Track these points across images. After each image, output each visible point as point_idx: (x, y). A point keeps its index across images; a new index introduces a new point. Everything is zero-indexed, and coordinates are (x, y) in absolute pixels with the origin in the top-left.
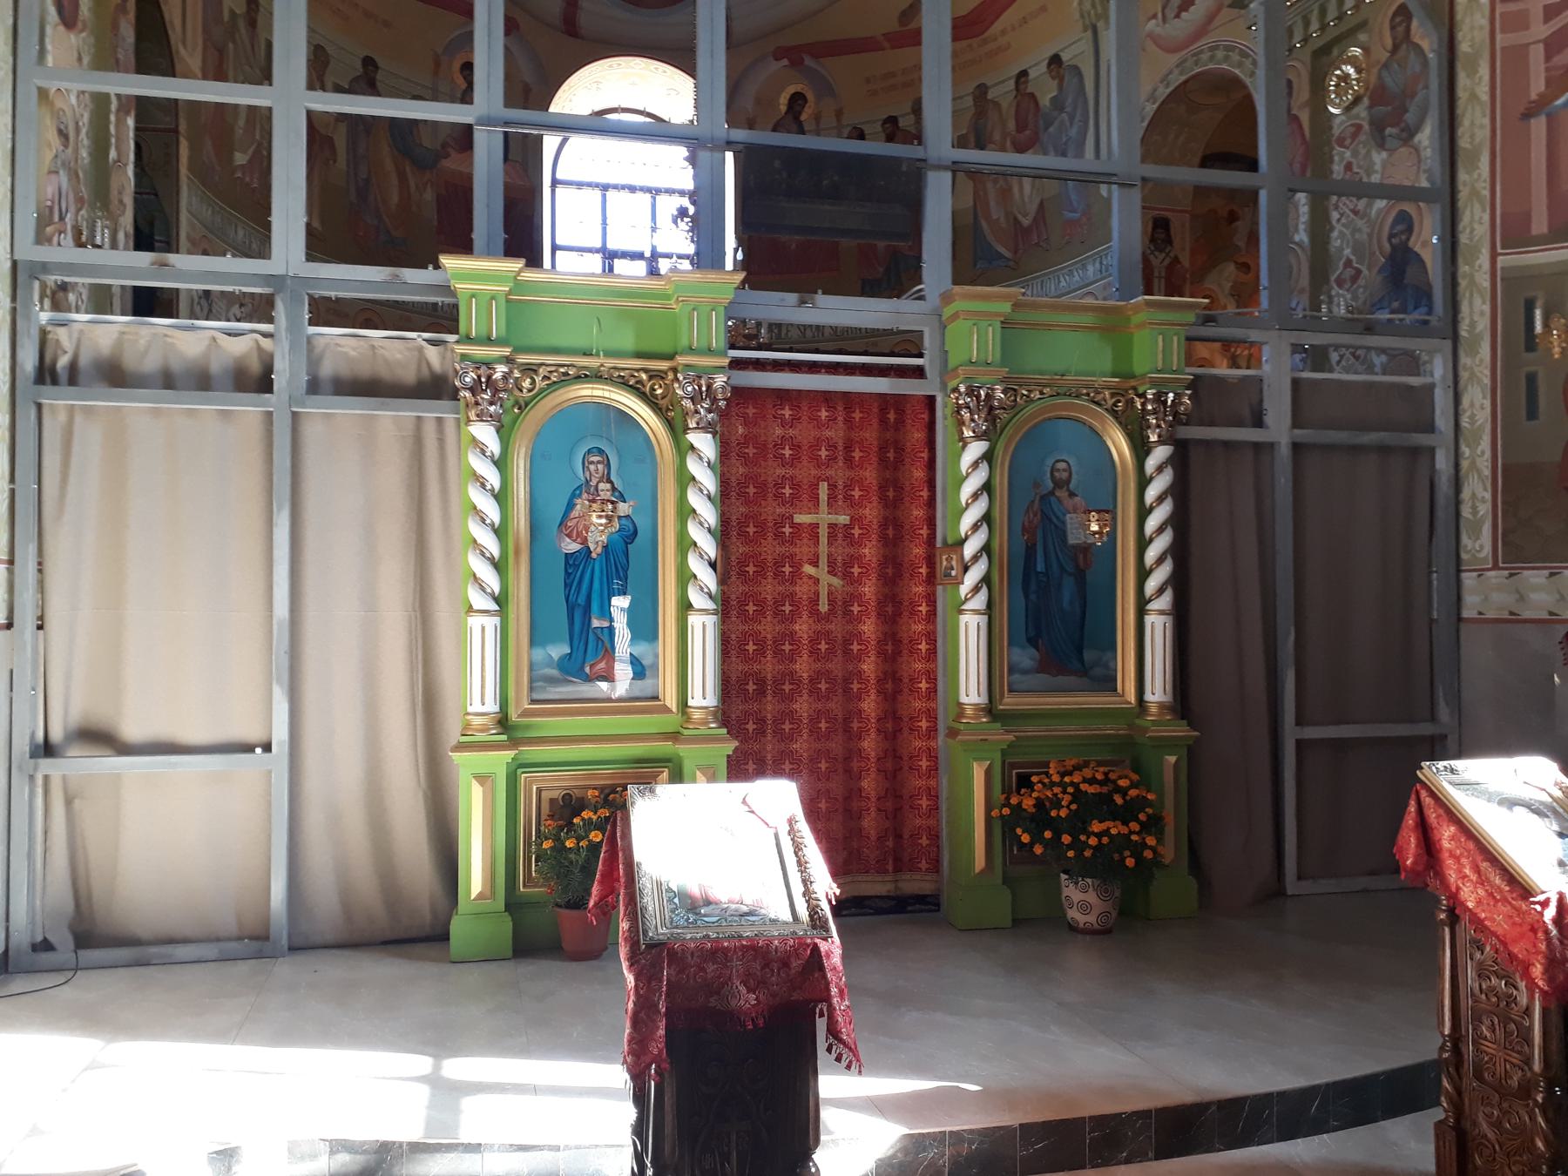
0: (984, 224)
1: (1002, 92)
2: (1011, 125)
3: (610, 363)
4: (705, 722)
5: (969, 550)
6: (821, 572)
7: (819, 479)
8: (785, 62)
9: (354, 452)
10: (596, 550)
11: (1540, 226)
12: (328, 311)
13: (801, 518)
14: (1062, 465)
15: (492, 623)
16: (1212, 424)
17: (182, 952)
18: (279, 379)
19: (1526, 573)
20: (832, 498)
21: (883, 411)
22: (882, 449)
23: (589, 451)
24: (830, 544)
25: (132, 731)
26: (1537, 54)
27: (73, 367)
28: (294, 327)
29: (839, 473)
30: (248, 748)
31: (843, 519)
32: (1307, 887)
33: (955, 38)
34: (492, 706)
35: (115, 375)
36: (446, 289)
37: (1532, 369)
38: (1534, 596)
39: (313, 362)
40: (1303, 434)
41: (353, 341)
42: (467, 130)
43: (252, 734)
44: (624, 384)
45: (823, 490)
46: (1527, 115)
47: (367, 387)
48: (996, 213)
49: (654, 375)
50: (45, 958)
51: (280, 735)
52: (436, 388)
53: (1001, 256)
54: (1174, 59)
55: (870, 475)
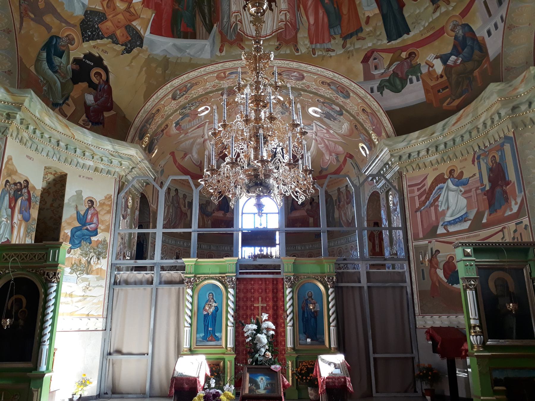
1: (343, 189)
2: (345, 197)
3: (214, 275)
4: (230, 351)
5: (288, 312)
9: (168, 294)
10: (210, 314)
11: (421, 236)
12: (163, 269)
13: (255, 305)
15: (188, 329)
16: (348, 282)
17: (130, 396)
18: (154, 282)
19: (443, 316)
20: (262, 301)
21: (273, 281)
22: (273, 290)
25: (125, 351)
26: (417, 198)
27: (120, 281)
28: (157, 272)
29: (264, 295)
30: (144, 354)
31: (265, 305)
32: (378, 395)
34: (188, 346)
35: (127, 283)
38: (428, 322)
39: (161, 278)
40: (369, 284)
42: (191, 233)
43: (145, 352)
44: (216, 279)
45: (260, 299)
46: (416, 212)
47: (170, 283)
48: (344, 219)
49: (223, 277)
50: (106, 396)
51: (150, 352)
52: (181, 282)
55: (270, 295)
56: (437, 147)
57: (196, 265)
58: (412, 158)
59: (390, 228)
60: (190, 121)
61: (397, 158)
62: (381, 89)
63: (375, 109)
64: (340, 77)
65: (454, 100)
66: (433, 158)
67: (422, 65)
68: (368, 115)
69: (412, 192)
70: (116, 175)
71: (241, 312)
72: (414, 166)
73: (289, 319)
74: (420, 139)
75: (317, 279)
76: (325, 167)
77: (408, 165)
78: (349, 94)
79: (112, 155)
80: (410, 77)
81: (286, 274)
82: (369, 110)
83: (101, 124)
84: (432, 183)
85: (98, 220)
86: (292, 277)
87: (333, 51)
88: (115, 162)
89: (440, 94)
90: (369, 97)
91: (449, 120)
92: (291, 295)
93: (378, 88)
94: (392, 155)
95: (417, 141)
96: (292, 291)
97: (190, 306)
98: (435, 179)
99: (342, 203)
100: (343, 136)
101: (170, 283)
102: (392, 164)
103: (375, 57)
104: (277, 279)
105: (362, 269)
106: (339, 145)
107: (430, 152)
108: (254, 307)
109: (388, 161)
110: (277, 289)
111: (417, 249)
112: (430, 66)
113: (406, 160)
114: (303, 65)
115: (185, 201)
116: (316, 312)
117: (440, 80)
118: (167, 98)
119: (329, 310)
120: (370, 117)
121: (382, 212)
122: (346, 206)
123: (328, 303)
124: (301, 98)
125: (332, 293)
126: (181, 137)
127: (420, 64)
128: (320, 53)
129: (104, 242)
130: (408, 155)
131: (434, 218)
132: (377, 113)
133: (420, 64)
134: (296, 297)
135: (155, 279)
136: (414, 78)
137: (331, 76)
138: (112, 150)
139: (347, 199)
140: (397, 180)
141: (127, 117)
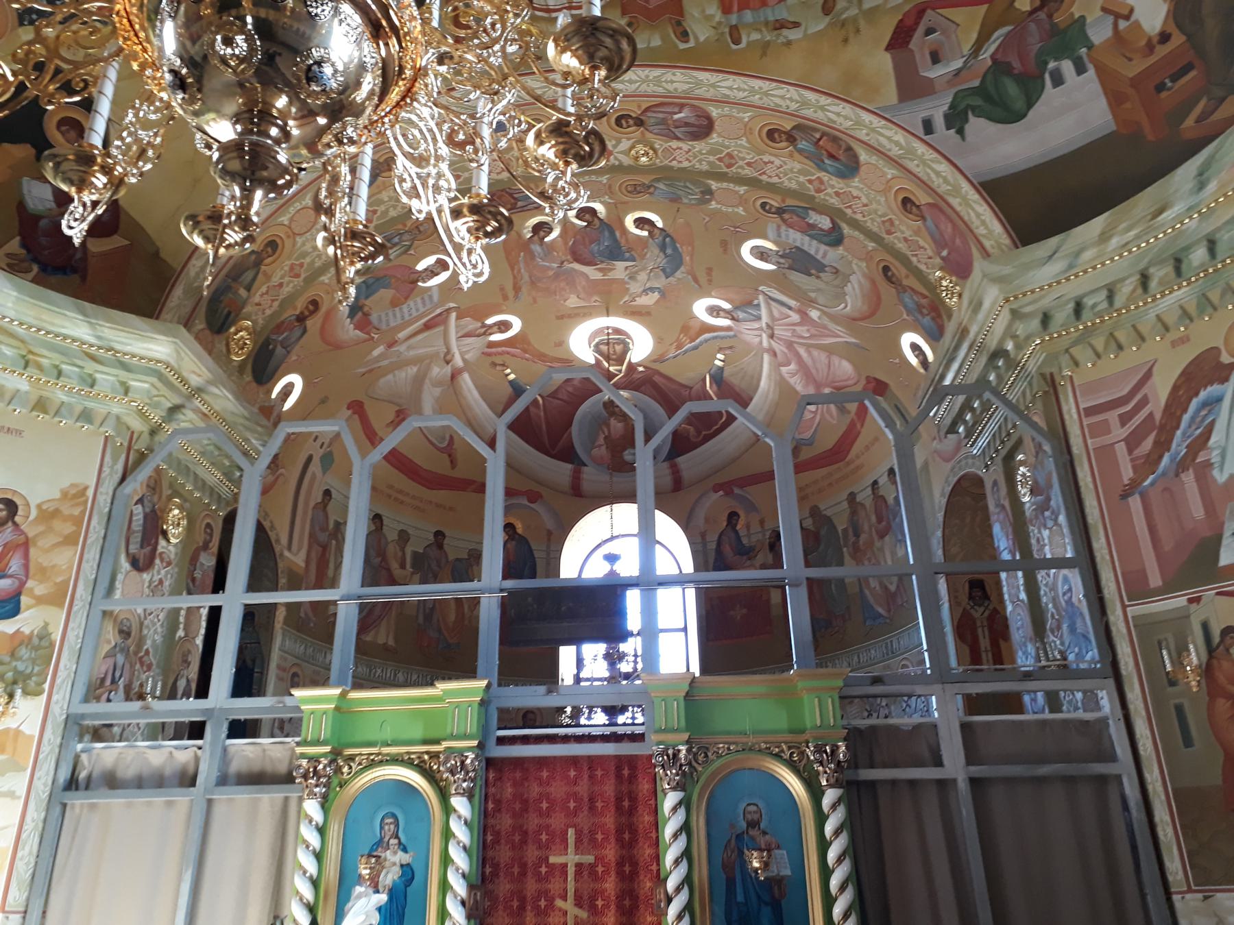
0: (867, 592)
1: (865, 496)
2: (874, 518)
3: (403, 749)
5: (671, 885)
6: (568, 905)
7: (568, 826)
8: (721, 493)
9: (244, 817)
11: (1155, 580)
13: (552, 860)
14: (753, 808)
16: (895, 765)
19: (1219, 895)
21: (619, 769)
22: (619, 800)
23: (382, 820)
24: (576, 881)
26: (1121, 449)
27: (89, 778)
28: (213, 744)
29: (583, 819)
31: (589, 859)
33: (796, 473)
35: (112, 782)
36: (298, 709)
37: (1177, 701)
40: (976, 770)
41: (251, 748)
46: (1125, 495)
47: (257, 779)
49: (434, 756)
53: (880, 615)
54: (950, 465)
55: (609, 821)
56: (1178, 263)
57: (342, 710)
58: (1086, 314)
59: (1030, 564)
60: (395, 303)
61: (1035, 323)
62: (956, 120)
63: (943, 188)
64: (824, 100)
65: (1222, 100)
66: (1170, 301)
67: (1088, 21)
68: (923, 218)
69: (1101, 429)
70: (111, 421)
71: (503, 887)
72: (1099, 343)
73: (673, 911)
74: (1115, 242)
75: (778, 756)
76: (807, 435)
77: (1075, 343)
78: (855, 158)
79: (93, 358)
80: (1052, 65)
81: (662, 737)
82: (922, 198)
83: (75, 271)
84: (1175, 388)
85: (26, 567)
86: (683, 748)
87: (796, 25)
88: (106, 378)
89: (1164, 94)
90: (921, 148)
91: (1217, 150)
92: (680, 816)
93: (947, 117)
94: (1015, 314)
95: (1099, 251)
96: (685, 803)
97: (311, 867)
98: (1183, 373)
99: (863, 537)
100: (851, 322)
101: (257, 779)
102: (1018, 347)
103: (931, 24)
104: (631, 761)
105: (940, 709)
106: (842, 357)
107: (1153, 284)
108: (548, 865)
109: (1002, 341)
110: (633, 799)
111: (1146, 629)
112: (1118, 16)
113: (1065, 326)
114: (703, 76)
115: (403, 550)
116: (775, 883)
117: (1162, 51)
118: (298, 206)
119: (826, 873)
120: (929, 222)
121: (997, 529)
122: (878, 544)
123: (823, 846)
124: (713, 205)
125: (834, 807)
126: (376, 353)
127: (1083, 18)
128: (755, 36)
129: (41, 638)
130: (1072, 305)
131: (1198, 512)
132: (951, 200)
133: (1083, 18)
134: (699, 824)
135: (203, 768)
136: (1067, 67)
137: (794, 106)
138: (93, 340)
139: (880, 520)
140: (1039, 404)
141: (163, 255)
